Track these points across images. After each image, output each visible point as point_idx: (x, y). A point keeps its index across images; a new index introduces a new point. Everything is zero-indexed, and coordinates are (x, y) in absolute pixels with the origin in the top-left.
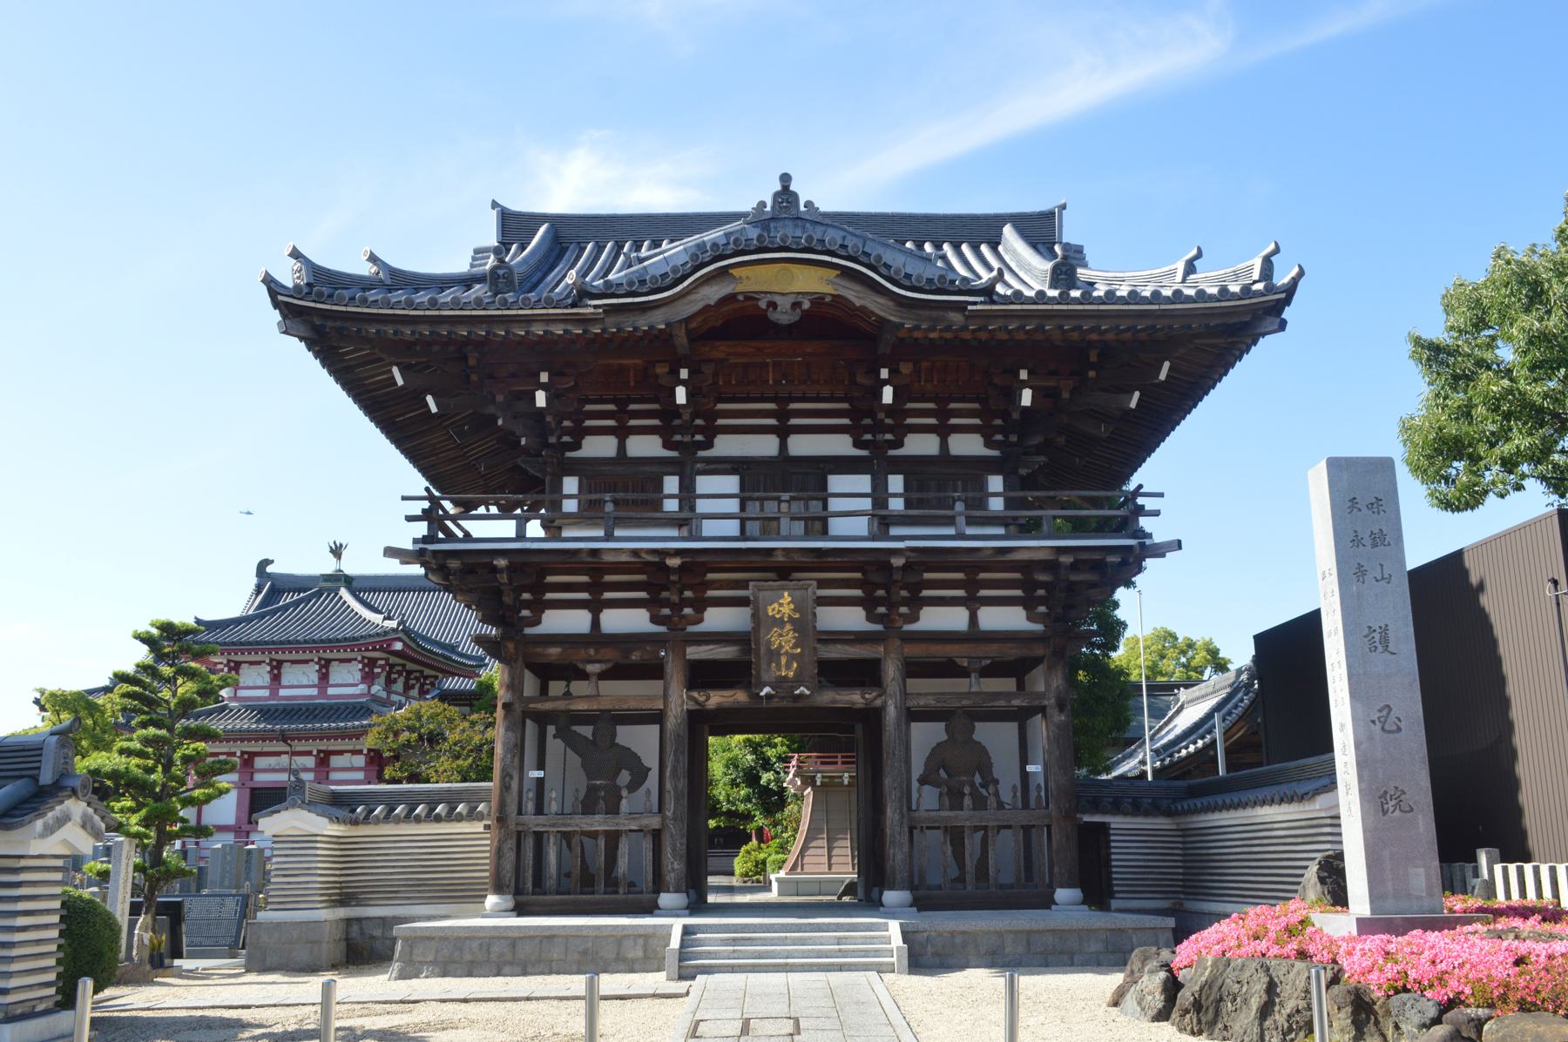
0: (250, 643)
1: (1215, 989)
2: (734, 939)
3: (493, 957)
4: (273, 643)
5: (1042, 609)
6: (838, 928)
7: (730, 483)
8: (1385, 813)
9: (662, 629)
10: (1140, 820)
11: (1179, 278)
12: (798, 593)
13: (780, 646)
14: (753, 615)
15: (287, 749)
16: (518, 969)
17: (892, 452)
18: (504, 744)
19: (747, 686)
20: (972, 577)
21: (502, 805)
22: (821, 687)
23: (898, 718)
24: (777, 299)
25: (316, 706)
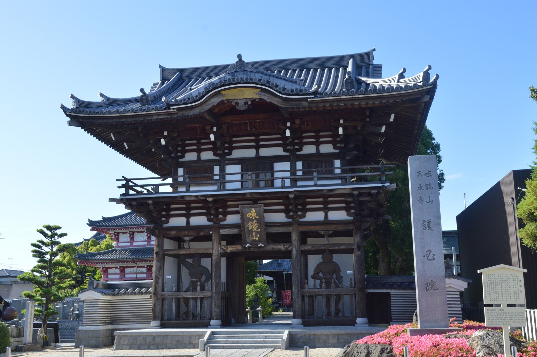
0: (121, 226)
1: (350, 355)
2: (228, 337)
3: (147, 342)
4: (129, 225)
5: (353, 211)
6: (267, 333)
7: (237, 168)
8: (427, 290)
9: (211, 223)
10: (402, 291)
11: (396, 81)
12: (258, 209)
13: (252, 229)
14: (241, 218)
15: (136, 265)
16: (156, 347)
17: (298, 153)
18: (156, 267)
19: (241, 244)
20: (326, 200)
21: (155, 289)
22: (268, 243)
23: (297, 254)
24: (239, 101)
25: (146, 249)
